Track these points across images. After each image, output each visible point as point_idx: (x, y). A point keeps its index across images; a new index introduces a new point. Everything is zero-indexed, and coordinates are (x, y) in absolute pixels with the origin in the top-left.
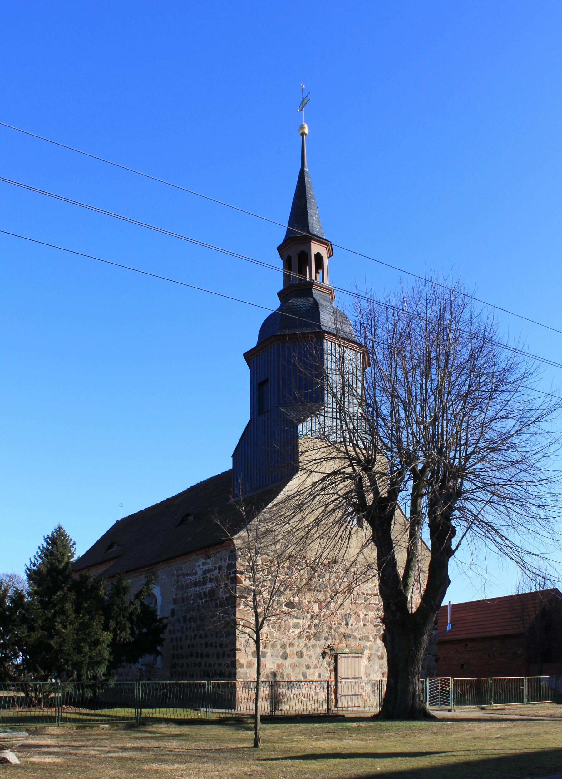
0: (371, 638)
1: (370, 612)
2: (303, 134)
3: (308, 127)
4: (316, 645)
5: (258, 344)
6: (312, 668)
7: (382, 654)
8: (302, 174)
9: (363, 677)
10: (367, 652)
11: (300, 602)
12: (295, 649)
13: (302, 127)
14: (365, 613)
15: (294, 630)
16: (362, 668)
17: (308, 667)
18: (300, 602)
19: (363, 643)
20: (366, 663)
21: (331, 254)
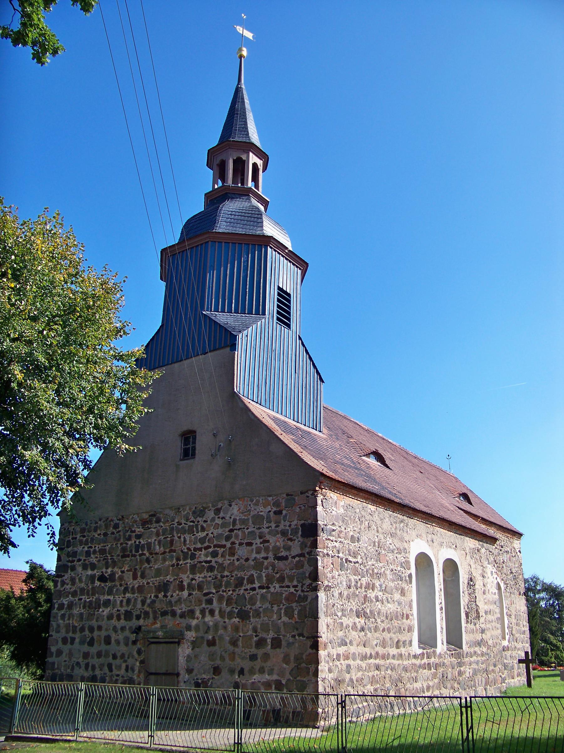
0: (198, 614)
1: (198, 575)
2: (241, 57)
3: (247, 51)
4: (125, 627)
5: (182, 240)
6: (119, 658)
7: (213, 637)
8: (238, 91)
9: (182, 672)
10: (190, 635)
11: (113, 574)
12: (103, 633)
13: (240, 50)
14: (191, 576)
15: (104, 609)
16: (182, 661)
17: (115, 657)
18: (113, 574)
19: (184, 622)
20: (188, 651)
21: (265, 169)
